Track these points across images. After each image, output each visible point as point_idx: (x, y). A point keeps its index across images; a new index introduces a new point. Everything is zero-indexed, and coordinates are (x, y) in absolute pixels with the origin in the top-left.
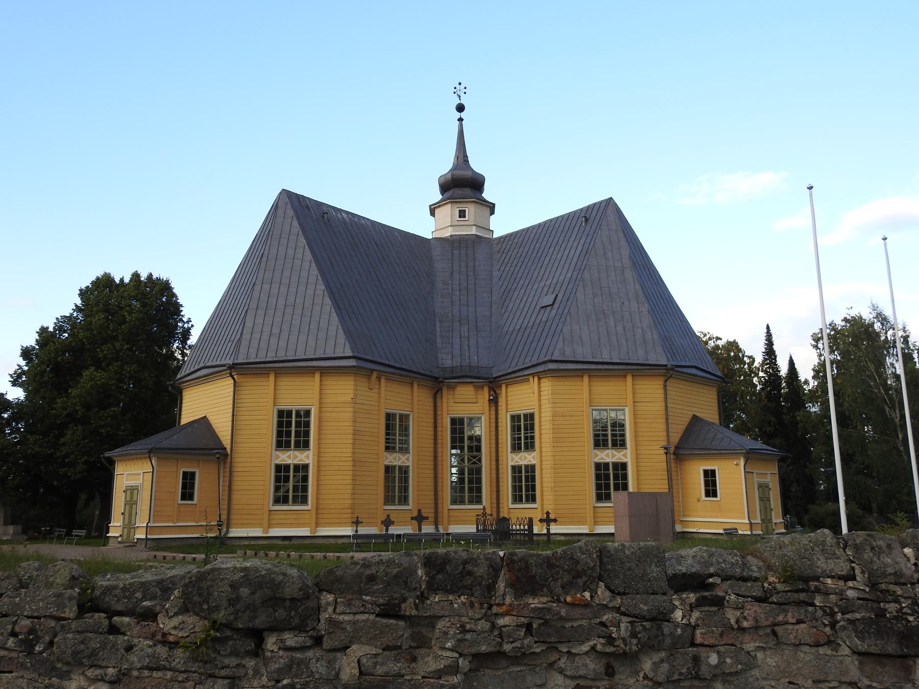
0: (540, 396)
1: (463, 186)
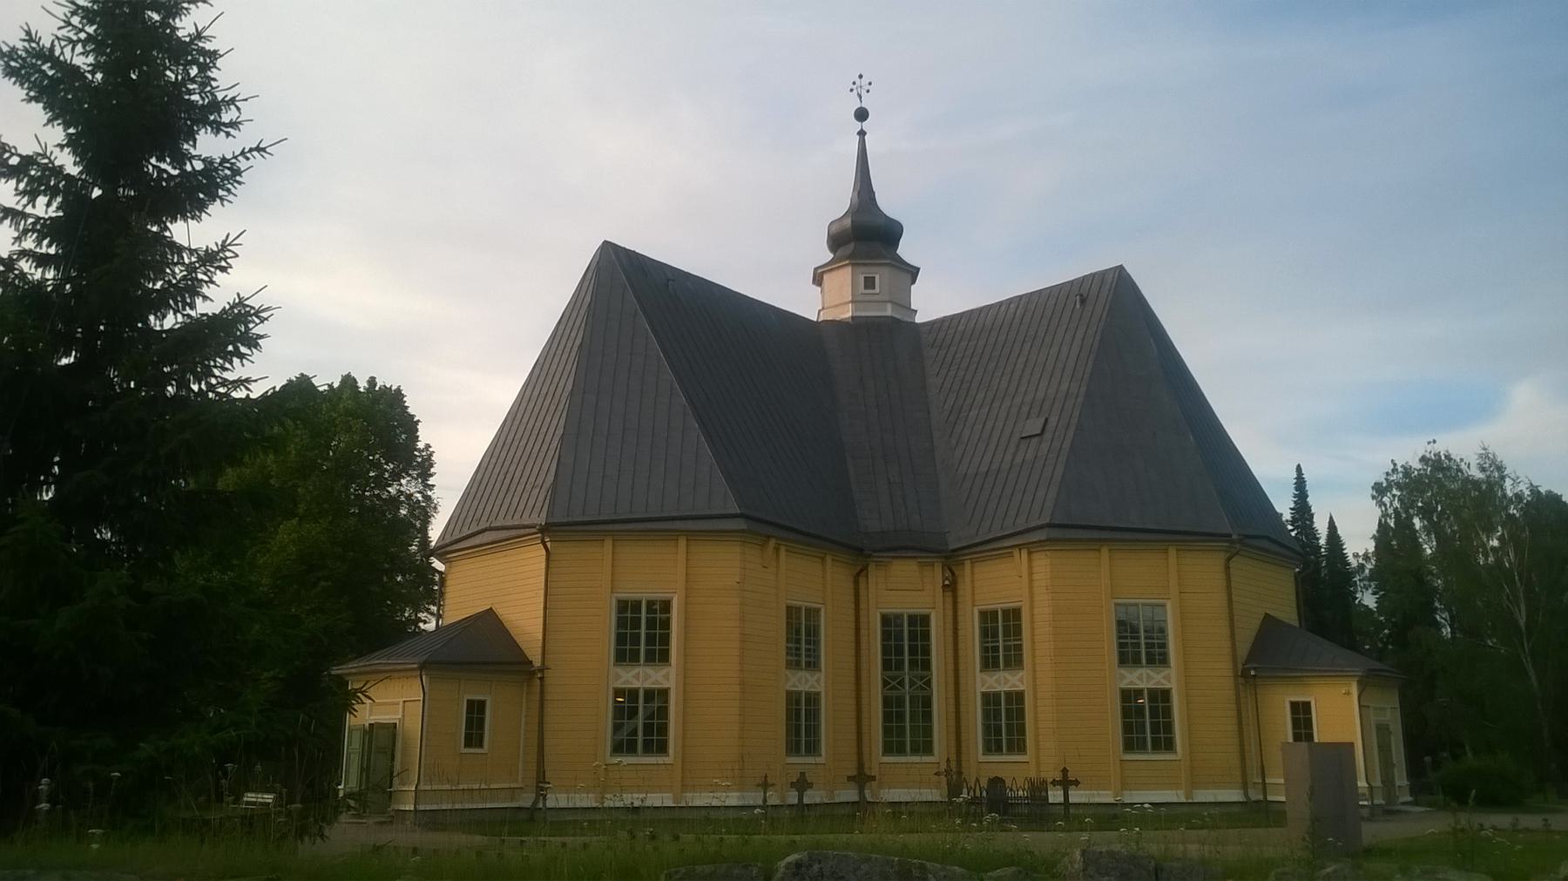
0: (1031, 581)
1: (867, 238)
